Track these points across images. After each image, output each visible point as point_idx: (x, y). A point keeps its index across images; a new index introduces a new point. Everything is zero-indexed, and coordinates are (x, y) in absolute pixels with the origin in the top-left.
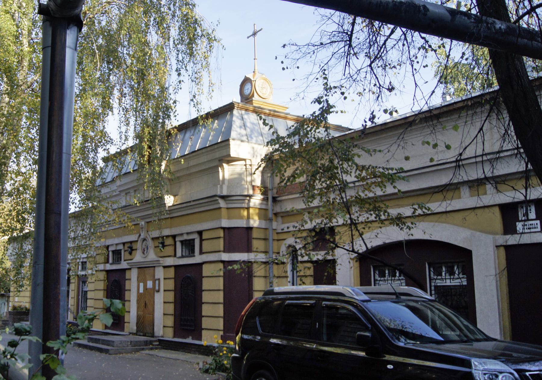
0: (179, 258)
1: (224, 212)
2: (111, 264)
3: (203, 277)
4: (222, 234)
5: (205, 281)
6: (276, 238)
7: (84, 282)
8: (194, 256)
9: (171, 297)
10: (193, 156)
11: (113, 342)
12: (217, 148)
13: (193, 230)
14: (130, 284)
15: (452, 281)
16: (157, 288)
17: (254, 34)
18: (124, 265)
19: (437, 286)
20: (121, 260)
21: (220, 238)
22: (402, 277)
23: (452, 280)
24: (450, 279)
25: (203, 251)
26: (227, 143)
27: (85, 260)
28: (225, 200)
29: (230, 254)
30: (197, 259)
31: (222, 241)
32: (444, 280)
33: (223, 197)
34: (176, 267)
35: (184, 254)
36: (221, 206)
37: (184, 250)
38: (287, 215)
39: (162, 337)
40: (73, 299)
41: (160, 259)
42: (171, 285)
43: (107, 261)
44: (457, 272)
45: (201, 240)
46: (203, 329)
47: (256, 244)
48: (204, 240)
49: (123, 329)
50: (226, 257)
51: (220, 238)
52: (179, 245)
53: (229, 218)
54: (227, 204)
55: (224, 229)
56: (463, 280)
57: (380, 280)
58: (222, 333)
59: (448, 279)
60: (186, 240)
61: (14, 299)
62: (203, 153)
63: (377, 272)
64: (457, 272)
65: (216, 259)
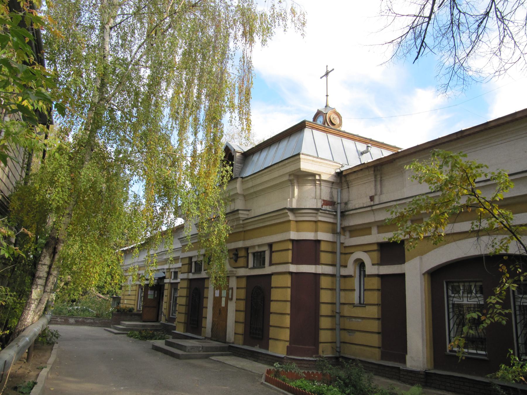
0: (251, 268)
1: (293, 225)
2: (193, 273)
3: (272, 288)
4: (290, 247)
5: (273, 291)
6: (344, 252)
7: (176, 289)
8: (264, 267)
9: (242, 305)
10: (265, 173)
11: (185, 347)
12: (288, 163)
13: (263, 243)
14: (208, 292)
15: (469, 300)
16: (230, 297)
17: (327, 74)
18: (203, 275)
19: (523, 305)
20: (201, 270)
21: (288, 250)
22: (478, 295)
23: (469, 299)
24: (467, 297)
25: (272, 263)
26: (297, 157)
27: (176, 270)
28: (294, 213)
29: (298, 266)
30: (268, 270)
31: (290, 252)
32: (462, 299)
33: (292, 210)
34: (248, 277)
35: (255, 266)
36: (290, 219)
37: (255, 261)
38: (355, 231)
39: (233, 343)
40: (166, 304)
41: (234, 270)
42: (243, 294)
43: (190, 271)
44: (474, 291)
45: (271, 252)
46: (270, 339)
47: (324, 257)
48: (273, 252)
49: (200, 333)
50: (293, 268)
51: (288, 250)
52: (251, 257)
53: (298, 231)
54: (296, 217)
55: (293, 241)
56: (480, 299)
57: (454, 297)
58: (288, 344)
59: (465, 297)
60: (257, 252)
61: (124, 301)
62: (274, 168)
63: (450, 288)
64: (474, 291)
65: (284, 270)
